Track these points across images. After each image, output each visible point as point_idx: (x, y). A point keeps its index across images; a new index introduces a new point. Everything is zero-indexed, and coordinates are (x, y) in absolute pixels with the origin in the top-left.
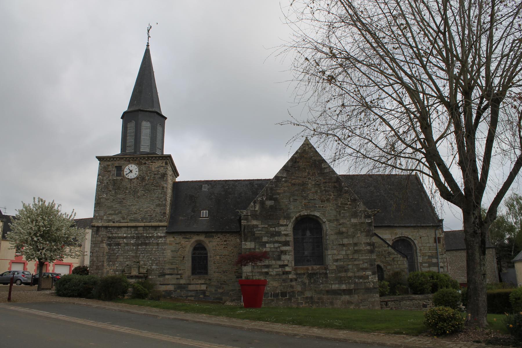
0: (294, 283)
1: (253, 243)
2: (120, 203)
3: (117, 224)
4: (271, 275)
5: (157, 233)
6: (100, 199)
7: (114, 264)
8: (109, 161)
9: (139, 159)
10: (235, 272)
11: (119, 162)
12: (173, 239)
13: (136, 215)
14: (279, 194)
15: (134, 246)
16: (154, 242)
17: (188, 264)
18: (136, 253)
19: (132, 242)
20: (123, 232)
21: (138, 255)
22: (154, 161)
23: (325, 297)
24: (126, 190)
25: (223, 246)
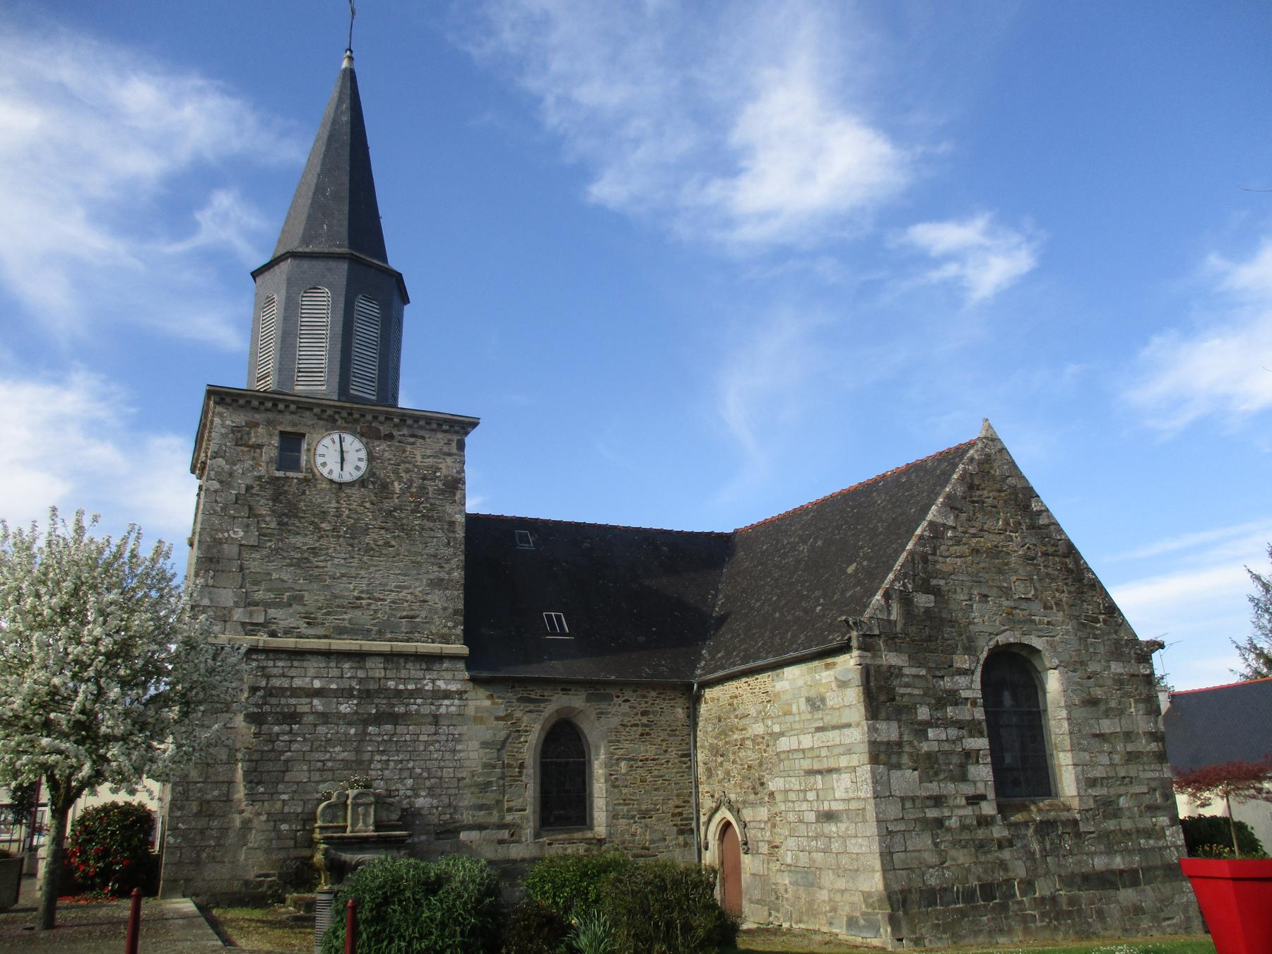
0: (1006, 854)
1: (895, 725)
2: (298, 566)
3: (290, 642)
4: (949, 829)
5: (433, 681)
6: (220, 542)
7: (272, 795)
8: (256, 409)
9: (369, 417)
10: (674, 815)
11: (296, 418)
12: (488, 703)
13: (358, 613)
14: (946, 576)
15: (350, 724)
16: (426, 710)
17: (527, 795)
18: (358, 751)
19: (344, 708)
20: (311, 672)
21: (366, 757)
22: (421, 433)
23: (1084, 895)
24: (323, 520)
25: (640, 730)
